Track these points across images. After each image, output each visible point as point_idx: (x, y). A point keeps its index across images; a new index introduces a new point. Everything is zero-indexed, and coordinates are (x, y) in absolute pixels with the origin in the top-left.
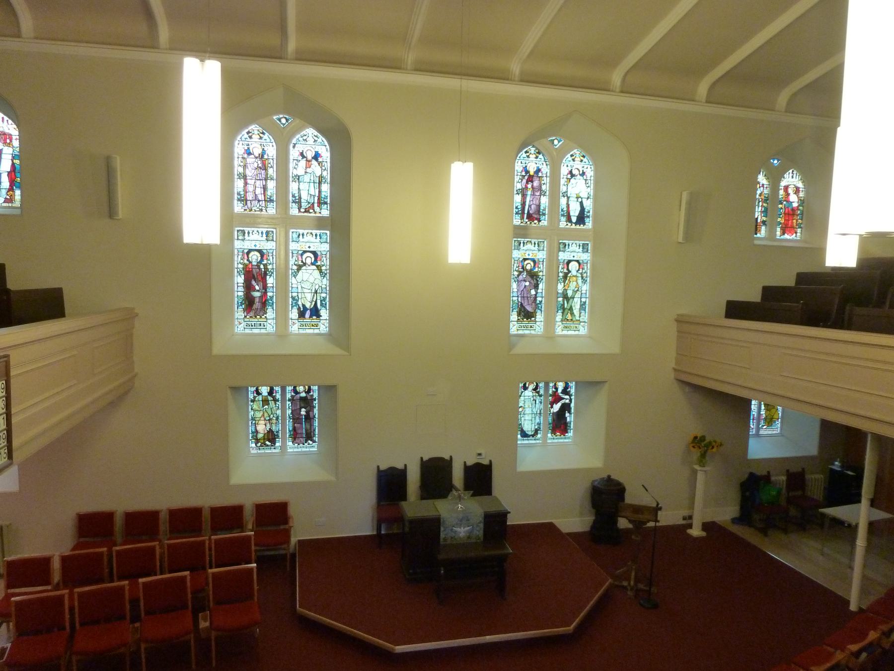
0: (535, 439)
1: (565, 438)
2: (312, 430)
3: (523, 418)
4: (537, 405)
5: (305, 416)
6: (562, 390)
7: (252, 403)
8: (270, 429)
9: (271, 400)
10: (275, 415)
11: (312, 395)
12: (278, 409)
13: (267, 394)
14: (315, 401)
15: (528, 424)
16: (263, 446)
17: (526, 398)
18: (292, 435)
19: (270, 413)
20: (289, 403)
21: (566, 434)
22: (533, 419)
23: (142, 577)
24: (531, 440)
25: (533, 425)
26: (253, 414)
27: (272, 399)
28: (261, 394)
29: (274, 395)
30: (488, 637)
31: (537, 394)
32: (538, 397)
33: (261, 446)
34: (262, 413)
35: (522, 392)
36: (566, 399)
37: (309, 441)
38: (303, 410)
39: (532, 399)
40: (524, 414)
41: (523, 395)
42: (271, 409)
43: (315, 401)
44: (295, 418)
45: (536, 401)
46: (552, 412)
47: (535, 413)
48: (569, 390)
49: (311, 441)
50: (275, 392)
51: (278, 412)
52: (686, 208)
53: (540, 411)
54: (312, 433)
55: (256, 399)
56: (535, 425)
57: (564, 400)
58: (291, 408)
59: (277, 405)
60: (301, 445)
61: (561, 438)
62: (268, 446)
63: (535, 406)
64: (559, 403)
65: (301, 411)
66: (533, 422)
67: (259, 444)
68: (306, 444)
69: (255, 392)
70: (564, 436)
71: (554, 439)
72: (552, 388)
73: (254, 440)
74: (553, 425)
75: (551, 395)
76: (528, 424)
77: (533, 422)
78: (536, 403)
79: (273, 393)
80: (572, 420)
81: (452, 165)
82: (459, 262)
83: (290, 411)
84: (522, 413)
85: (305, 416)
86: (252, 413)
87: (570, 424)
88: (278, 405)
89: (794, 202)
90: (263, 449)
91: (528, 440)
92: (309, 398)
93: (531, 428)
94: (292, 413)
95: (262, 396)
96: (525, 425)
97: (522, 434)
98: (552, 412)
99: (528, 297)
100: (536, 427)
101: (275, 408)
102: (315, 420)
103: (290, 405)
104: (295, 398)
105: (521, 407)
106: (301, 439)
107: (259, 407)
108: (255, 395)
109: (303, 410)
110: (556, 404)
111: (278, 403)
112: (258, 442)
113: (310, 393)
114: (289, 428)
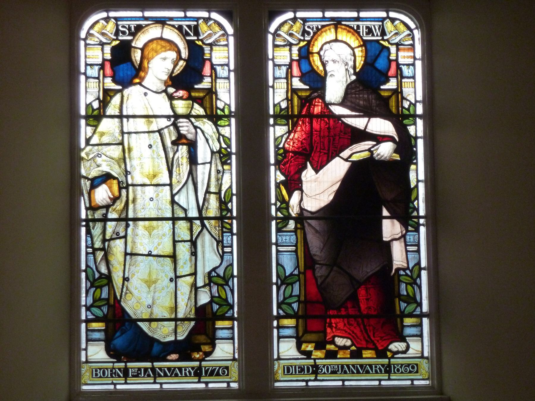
0: (198, 373)
1: (388, 370)
3: (118, 246)
4: (202, 172)
6: (350, 89)
15: (150, 283)
17: (130, 125)
21: (396, 346)
22: (183, 250)
23: (103, 104)
24: (172, 372)
25: (185, 284)
31: (198, 110)
32: (208, 126)
35: (108, 94)
36: (379, 139)
39: (170, 136)
40: (124, 219)
41: (112, 109)
45: (192, 146)
46: (294, 211)
47: (193, 213)
48: (392, 84)
50: (207, 70)
53: (223, 204)
56: (195, 288)
57: (368, 144)
61: (365, 370)
63: (192, 174)
64: (337, 161)
66: (185, 268)
70: (381, 354)
71: (316, 370)
72: (289, 76)
73: (290, 322)
74: (305, 286)
76: (150, 283)
77: (185, 268)
78: (193, 160)
80: (424, 264)
81: (274, 321)
82: (272, 225)
84: (112, 215)
87: (415, 282)
91: (155, 374)
93: (168, 302)
96: (135, 284)
97: (119, 342)
98: (294, 211)
99: (177, 116)
100: (204, 298)
105: (106, 177)
110: (317, 170)
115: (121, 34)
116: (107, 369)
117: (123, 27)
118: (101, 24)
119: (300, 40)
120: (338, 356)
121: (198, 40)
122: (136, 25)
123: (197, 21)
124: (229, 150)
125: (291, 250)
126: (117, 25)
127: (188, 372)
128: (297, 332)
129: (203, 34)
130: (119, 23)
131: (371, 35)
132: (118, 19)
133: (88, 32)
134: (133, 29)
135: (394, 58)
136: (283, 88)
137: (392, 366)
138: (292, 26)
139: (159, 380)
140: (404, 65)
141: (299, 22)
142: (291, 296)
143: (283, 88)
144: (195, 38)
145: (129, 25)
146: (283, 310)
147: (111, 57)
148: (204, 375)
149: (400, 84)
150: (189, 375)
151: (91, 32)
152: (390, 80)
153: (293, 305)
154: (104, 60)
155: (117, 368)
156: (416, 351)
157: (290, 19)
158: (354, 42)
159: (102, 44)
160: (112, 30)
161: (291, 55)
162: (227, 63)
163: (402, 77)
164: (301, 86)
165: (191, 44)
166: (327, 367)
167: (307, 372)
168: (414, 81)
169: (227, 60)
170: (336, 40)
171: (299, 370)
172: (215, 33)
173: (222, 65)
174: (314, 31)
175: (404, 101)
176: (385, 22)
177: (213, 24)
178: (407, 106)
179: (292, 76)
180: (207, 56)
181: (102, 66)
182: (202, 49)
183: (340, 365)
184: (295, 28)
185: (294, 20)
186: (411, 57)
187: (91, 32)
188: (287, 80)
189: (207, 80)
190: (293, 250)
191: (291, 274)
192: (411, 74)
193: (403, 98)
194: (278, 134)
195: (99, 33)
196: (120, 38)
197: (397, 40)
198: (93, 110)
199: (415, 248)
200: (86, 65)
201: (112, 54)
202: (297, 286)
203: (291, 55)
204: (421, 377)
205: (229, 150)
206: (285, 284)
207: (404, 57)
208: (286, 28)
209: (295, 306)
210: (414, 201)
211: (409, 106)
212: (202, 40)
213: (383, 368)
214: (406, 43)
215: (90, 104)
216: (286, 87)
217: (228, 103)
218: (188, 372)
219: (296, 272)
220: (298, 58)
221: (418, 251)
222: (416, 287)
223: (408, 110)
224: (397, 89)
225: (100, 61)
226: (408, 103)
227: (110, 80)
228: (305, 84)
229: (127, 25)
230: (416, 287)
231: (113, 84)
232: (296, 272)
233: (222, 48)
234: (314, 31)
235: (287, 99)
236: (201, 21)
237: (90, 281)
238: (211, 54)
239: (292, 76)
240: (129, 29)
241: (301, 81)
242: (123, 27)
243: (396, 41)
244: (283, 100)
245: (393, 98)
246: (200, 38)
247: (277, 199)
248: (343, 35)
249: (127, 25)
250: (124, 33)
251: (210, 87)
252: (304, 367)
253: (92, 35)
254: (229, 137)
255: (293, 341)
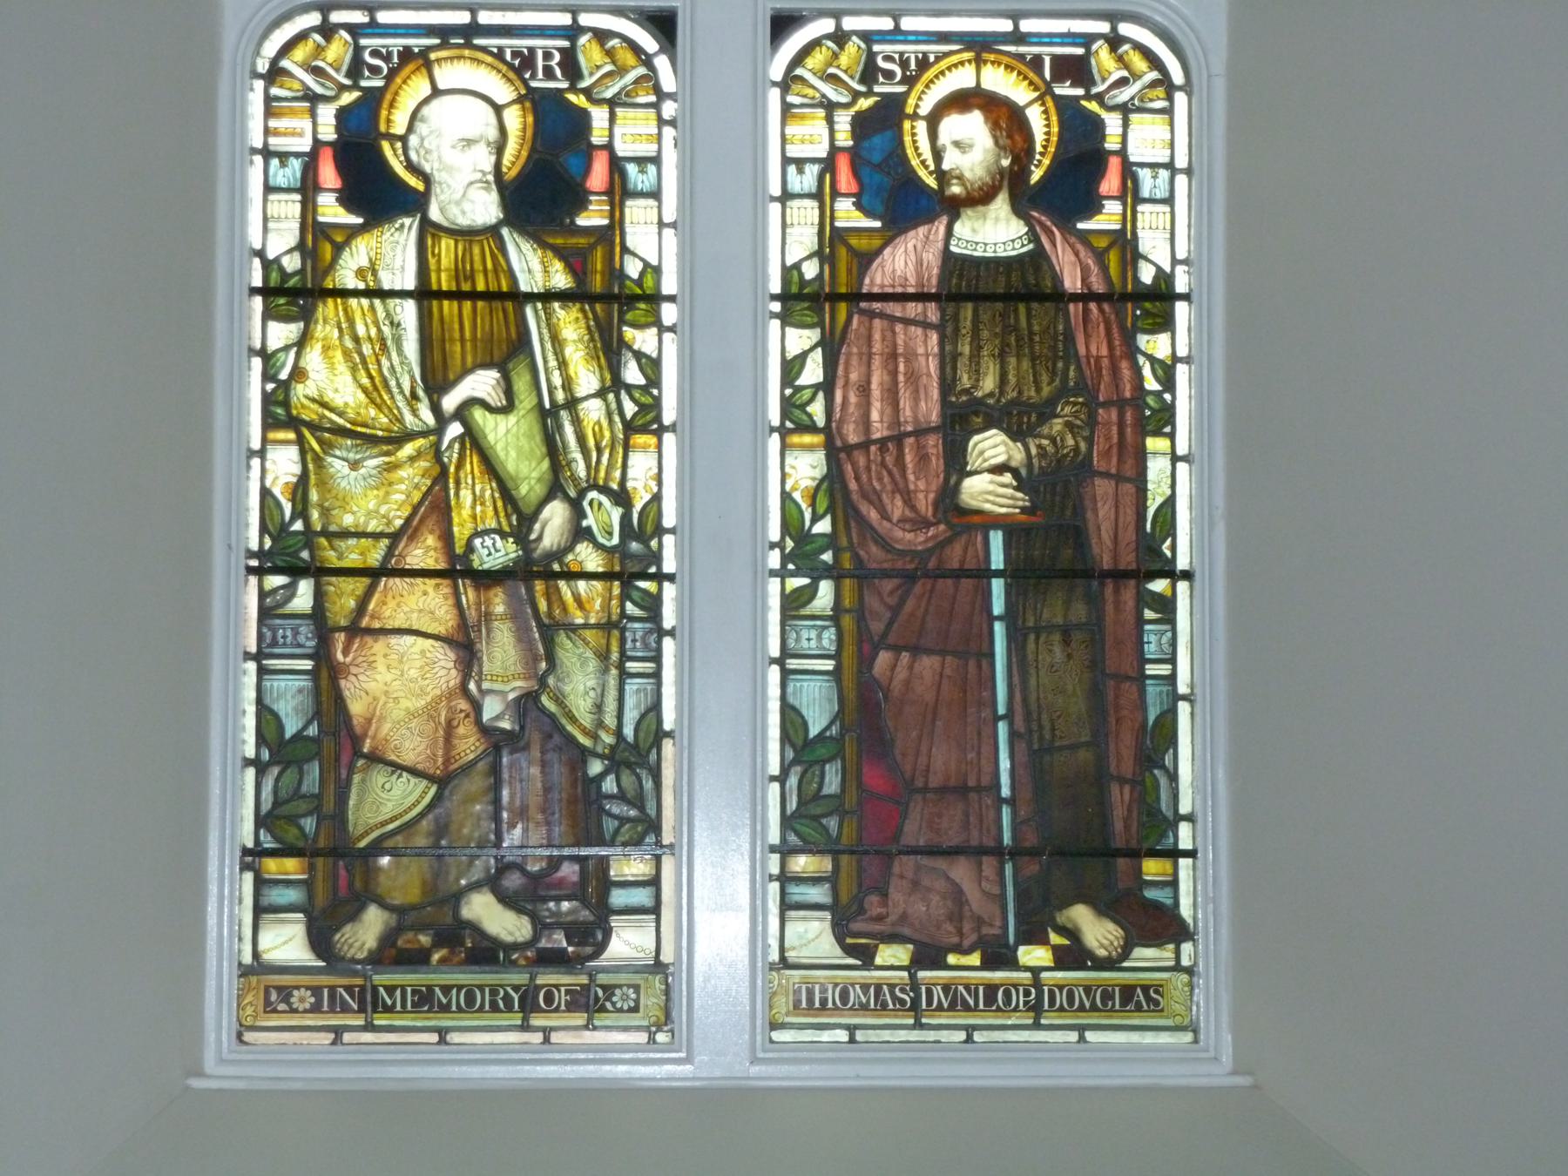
2: (1123, 758)
5: (1014, 531)
7: (281, 334)
8: (526, 705)
9: (548, 297)
10: (604, 516)
11: (1125, 244)
12: (647, 421)
13: (485, 208)
14: (1165, 323)
16: (418, 959)
18: (837, 805)
19: (528, 473)
20: (801, 339)
26: (299, 490)
27: (561, 279)
28: (415, 202)
29: (593, 217)
30: (1007, 873)
33: (390, 953)
34: (411, 478)
37: (1081, 915)
38: (991, 446)
42: (547, 417)
43: (1165, 323)
44: (874, 555)
49: (1105, 909)
50: (598, 177)
51: (641, 468)
52: (249, 414)
54: (1120, 796)
55: (346, 275)
58: (817, 410)
59: (632, 374)
60: (966, 966)
62: (487, 952)
65: (957, 464)
67: (367, 931)
68: (1034, 955)
69: (329, 175)
73: (290, 867)
75: (774, 297)
79: (580, 200)
83: (807, 467)
85: (1014, 531)
86: (284, 464)
88: (651, 366)
89: (635, 255)
90: (424, 1000)
92: (1072, 282)
94: (833, 489)
95: (429, 231)
101: (593, 411)
102: (1166, 606)
103: (813, 373)
104: (878, 278)
106: (961, 871)
107: (375, 391)
108: (331, 210)
109: (991, 446)
111: (644, 340)
112: (346, 907)
113: (1092, 206)
114: (789, 712)
115: (367, 73)
116: (1015, 986)
117: (375, 53)
118: (310, 43)
119: (342, 88)
120: (878, 961)
121: (1088, 97)
122: (401, 49)
123: (1087, 46)
124: (1167, 397)
125: (641, 670)
126: (358, 50)
127: (502, 999)
128: (311, 896)
129: (1104, 80)
130: (363, 42)
131: (1068, 84)
132: (359, 31)
133: (274, 62)
134: (913, 66)
135: (1117, 147)
136: (1161, 227)
137: (923, 988)
138: (835, 56)
139: (537, 1020)
140: (1142, 165)
141: (854, 47)
142: (297, 795)
143: (809, 222)
144: (1080, 92)
145: (901, 54)
146: (797, 834)
147: (336, 136)
148: (1046, 1007)
149: (1130, 216)
150: (1068, 1005)
151: (799, 71)
152: (1103, 206)
153: (302, 821)
154: (834, 149)
155: (508, 985)
156: (629, 944)
157: (828, 37)
158: (503, 92)
159: (830, 107)
160: (854, 67)
161: (832, 132)
162: (654, 154)
163: (1138, 200)
164: (336, 216)
165: (537, 103)
166: (1004, 991)
167: (1049, 1007)
168: (656, 204)
169: (655, 147)
170: (436, 92)
171: (413, 1001)
172: (1137, 76)
173: (1153, 166)
174: (911, 71)
175: (628, 259)
176: (1094, 47)
177: (1131, 52)
178: (635, 275)
179: (317, 189)
180: (1112, 143)
181: (828, 165)
182: (584, 116)
183: (1117, 986)
184: (844, 60)
185: (840, 38)
186: (276, 133)
187: (799, 71)
188: (612, 204)
189: (1113, 208)
190: (648, 671)
191: (298, 736)
192: (1161, 193)
193: (625, 250)
194: (793, 350)
195: (305, 67)
196: (364, 83)
197: (1124, 95)
198: (285, 275)
199: (649, 666)
200: (786, 161)
201: (338, 129)
202: (314, 771)
203: (832, 132)
204: (1169, 1022)
205: (1167, 397)
206: (278, 763)
207: (293, 133)
208: (816, 60)
209: (309, 824)
210: (652, 537)
211: (642, 274)
212: (587, 92)
213: (517, 993)
214: (641, 100)
215: (797, 266)
216: (816, 221)
217: (655, 262)
218: (502, 999)
219: (313, 731)
220: (851, 143)
221: (657, 675)
222: (644, 774)
223: (639, 282)
224: (1123, 231)
225: (822, 151)
226: (640, 266)
227: (333, 199)
228: (868, 213)
229: (896, 53)
230: (644, 774)
231: (341, 211)
232: (313, 731)
233: (641, 113)
234: (911, 71)
235: (819, 254)
236: (584, 39)
237: (793, 746)
238: (1124, 136)
239: (835, 194)
240: (904, 64)
241: (859, 206)
242: (888, 58)
243: (608, 94)
244: (290, 251)
245: (599, 253)
246: (1095, 90)
247: (785, 527)
248: (451, 73)
249: (896, 53)
250: (889, 75)
251: (1118, 227)
252: (1114, 990)
253: (285, 72)
254: (654, 355)
255: (296, 922)
